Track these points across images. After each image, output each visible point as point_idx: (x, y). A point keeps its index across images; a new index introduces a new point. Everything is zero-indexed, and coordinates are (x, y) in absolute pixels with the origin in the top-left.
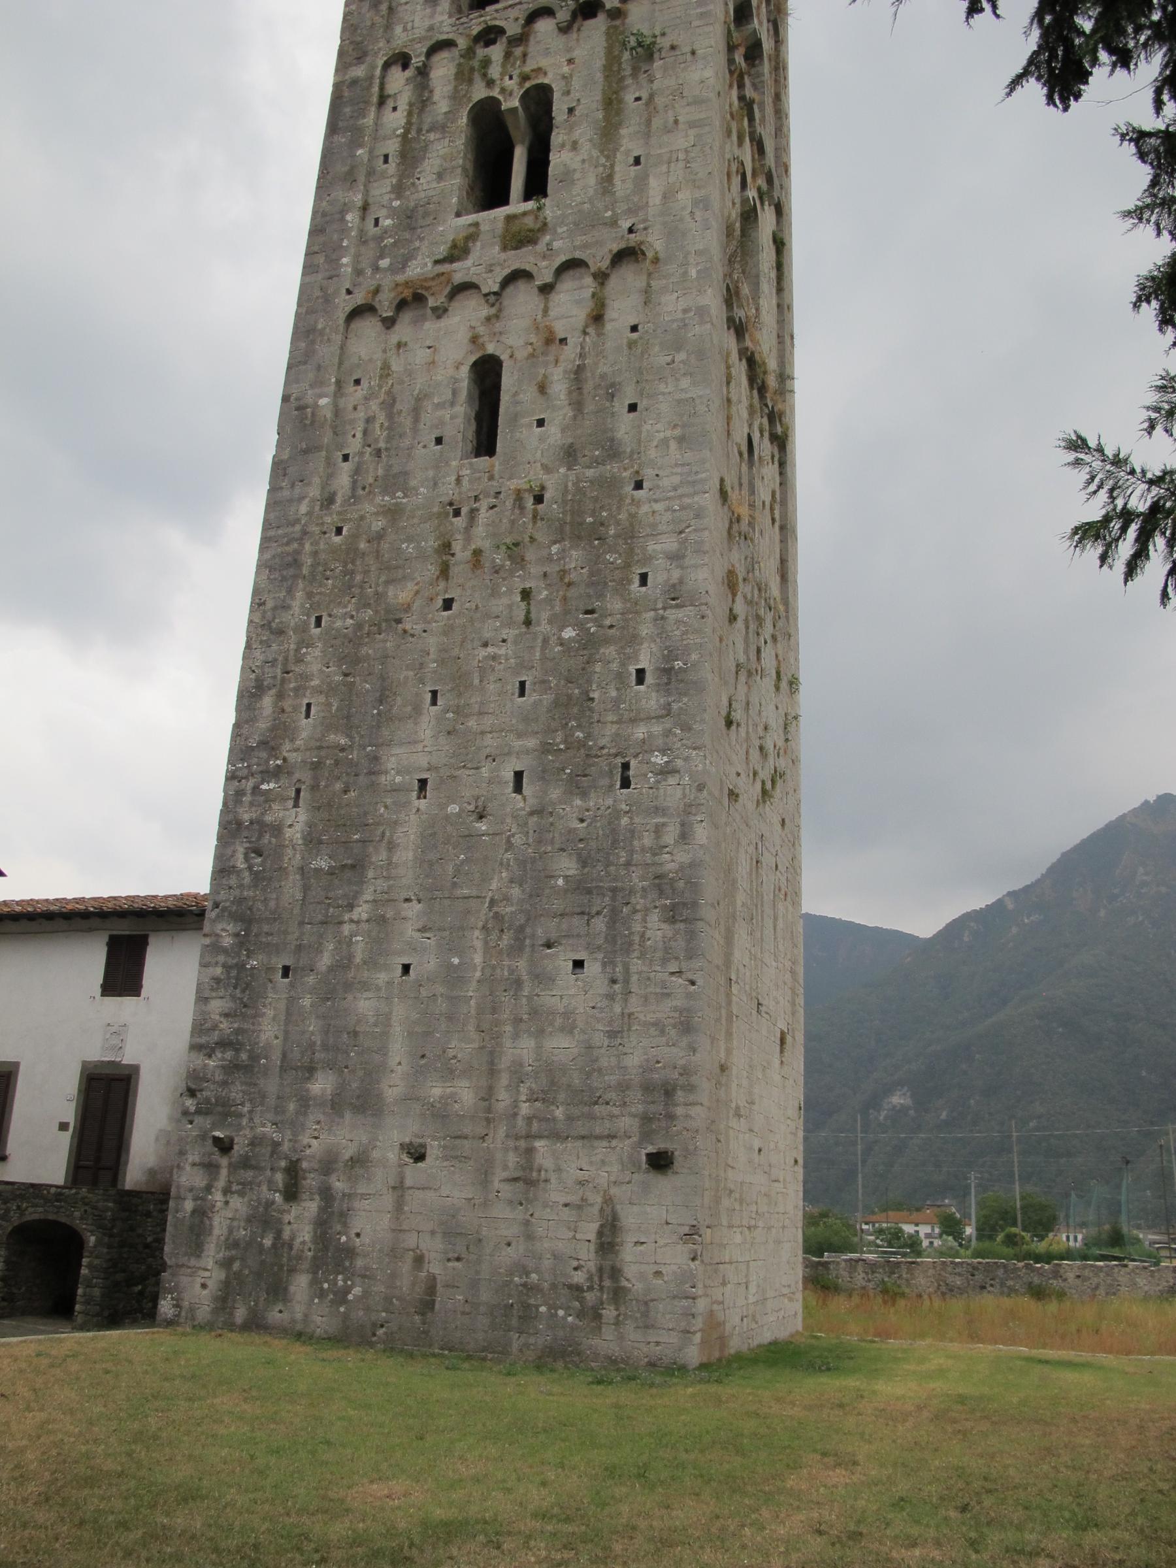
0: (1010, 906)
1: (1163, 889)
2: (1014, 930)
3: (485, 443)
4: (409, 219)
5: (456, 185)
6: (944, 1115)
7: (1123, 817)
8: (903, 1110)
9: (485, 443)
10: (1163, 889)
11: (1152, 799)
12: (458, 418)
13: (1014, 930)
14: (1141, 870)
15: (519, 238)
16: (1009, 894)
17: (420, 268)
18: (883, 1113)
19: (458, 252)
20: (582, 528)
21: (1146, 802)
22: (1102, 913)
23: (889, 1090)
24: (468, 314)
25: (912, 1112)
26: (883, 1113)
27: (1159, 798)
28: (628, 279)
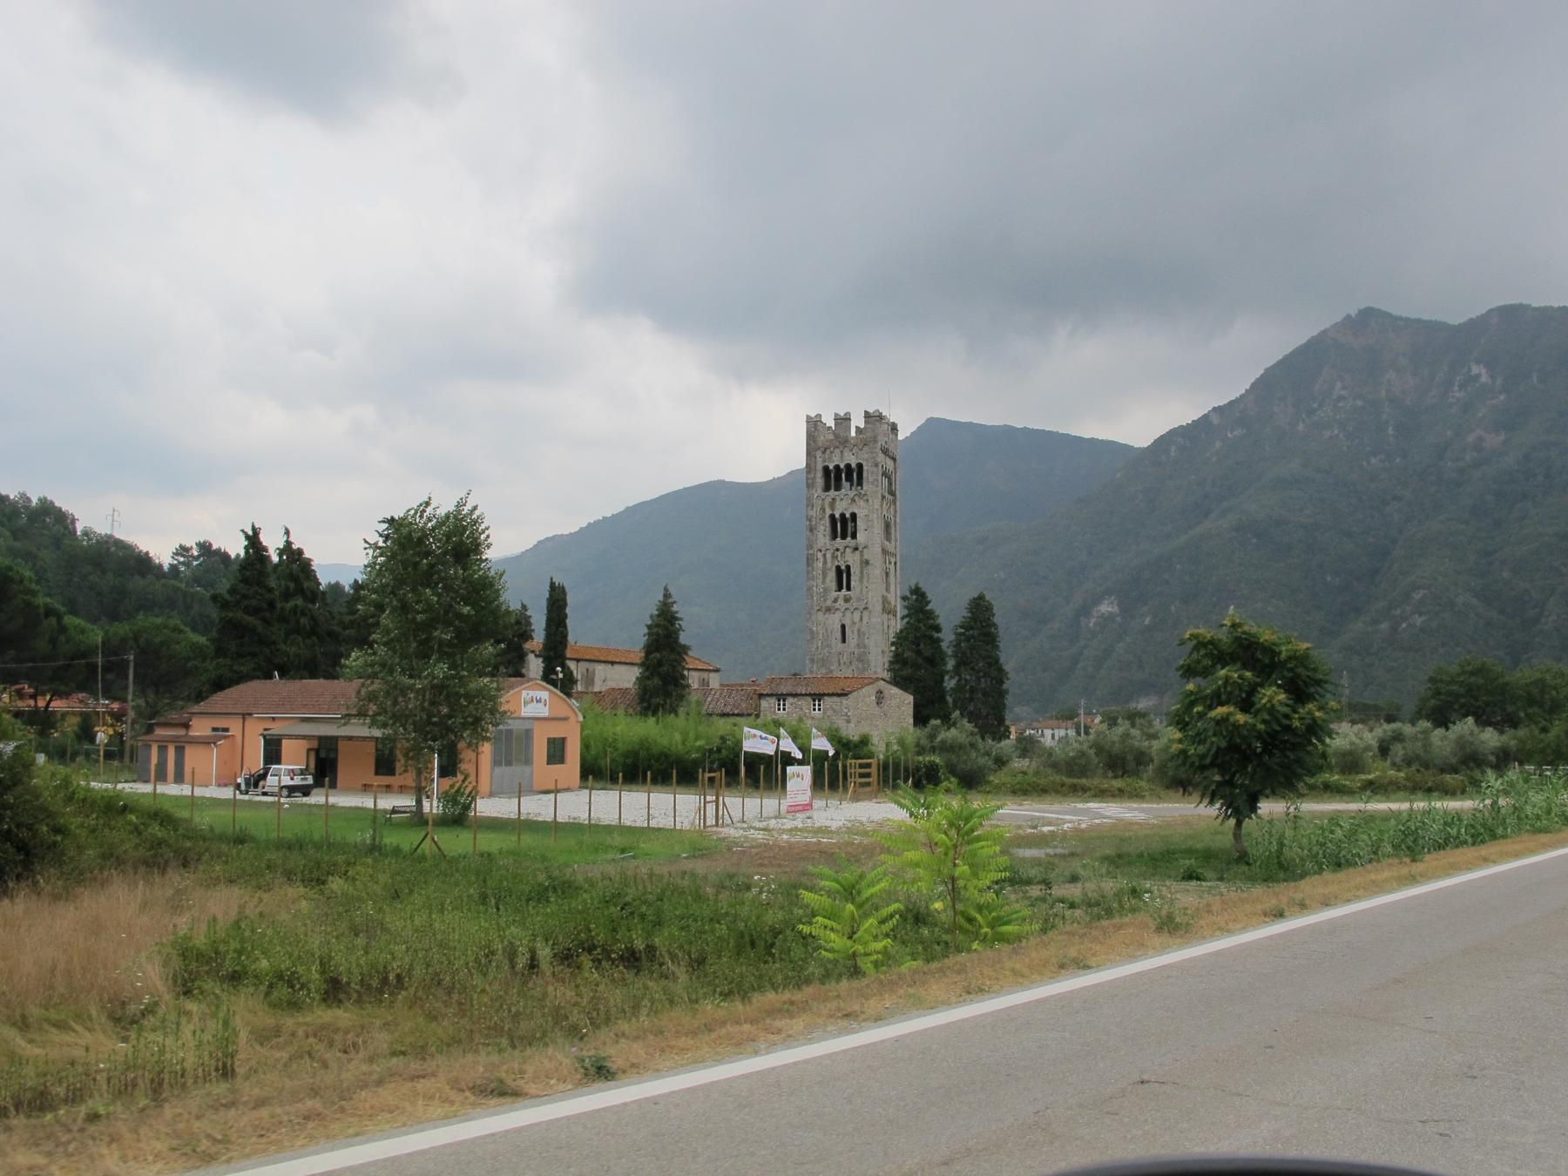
0: (1215, 420)
1: (1359, 403)
2: (1218, 444)
3: (844, 640)
4: (826, 590)
5: (834, 585)
6: (1147, 621)
7: (1325, 332)
8: (1110, 618)
9: (844, 640)
10: (1359, 403)
11: (1353, 313)
12: (839, 635)
13: (1218, 444)
14: (1339, 384)
15: (847, 600)
16: (1215, 409)
17: (829, 603)
18: (1093, 620)
19: (835, 601)
20: (860, 660)
21: (1348, 317)
22: (1301, 427)
23: (1097, 600)
24: (838, 615)
25: (1118, 619)
26: (1093, 620)
27: (1360, 311)
28: (866, 613)
